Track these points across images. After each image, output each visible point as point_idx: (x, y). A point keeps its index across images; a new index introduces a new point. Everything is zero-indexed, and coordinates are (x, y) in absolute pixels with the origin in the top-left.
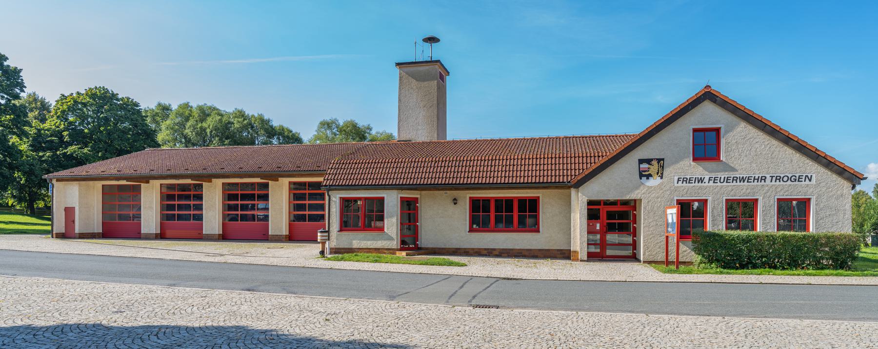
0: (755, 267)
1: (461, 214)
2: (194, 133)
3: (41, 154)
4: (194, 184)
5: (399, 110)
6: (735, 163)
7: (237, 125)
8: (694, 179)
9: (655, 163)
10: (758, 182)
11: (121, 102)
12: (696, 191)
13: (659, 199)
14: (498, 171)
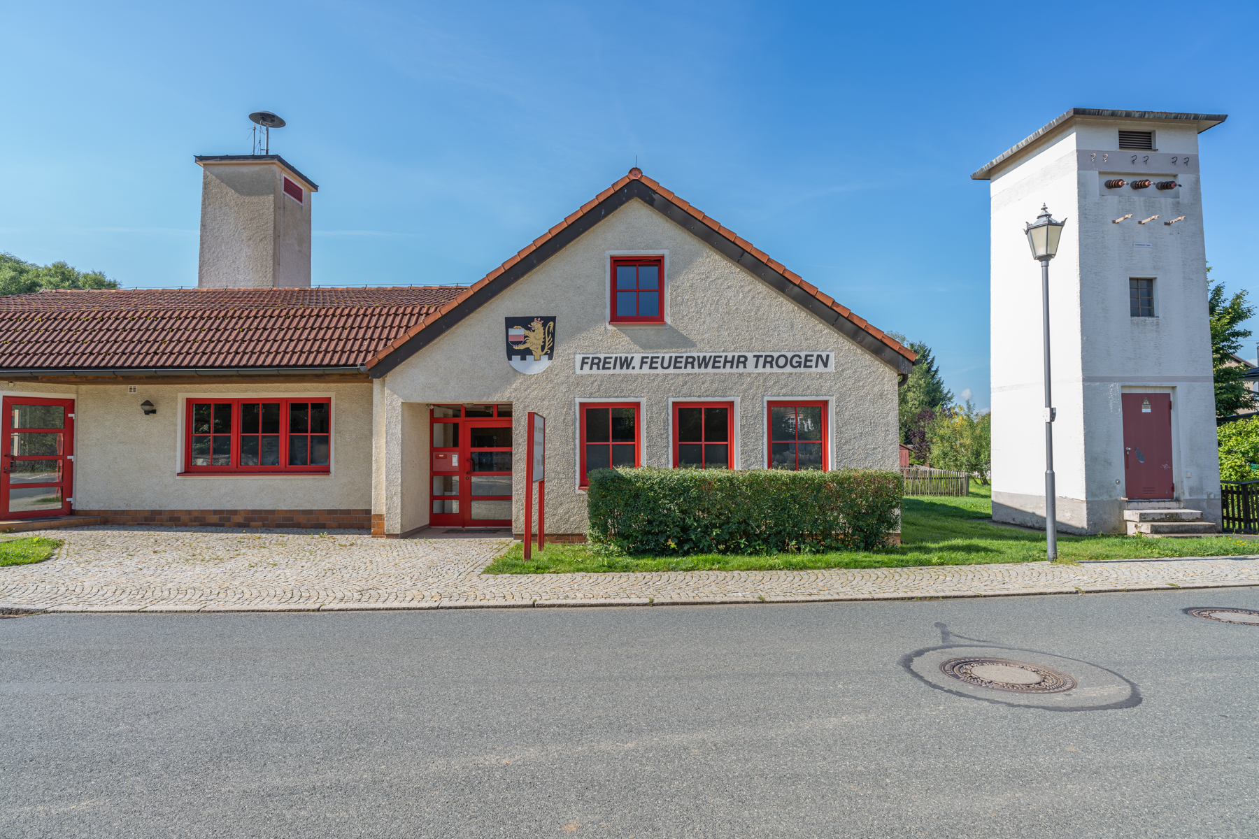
6: (690, 327)
8: (612, 361)
9: (537, 325)
10: (732, 367)
13: (546, 403)
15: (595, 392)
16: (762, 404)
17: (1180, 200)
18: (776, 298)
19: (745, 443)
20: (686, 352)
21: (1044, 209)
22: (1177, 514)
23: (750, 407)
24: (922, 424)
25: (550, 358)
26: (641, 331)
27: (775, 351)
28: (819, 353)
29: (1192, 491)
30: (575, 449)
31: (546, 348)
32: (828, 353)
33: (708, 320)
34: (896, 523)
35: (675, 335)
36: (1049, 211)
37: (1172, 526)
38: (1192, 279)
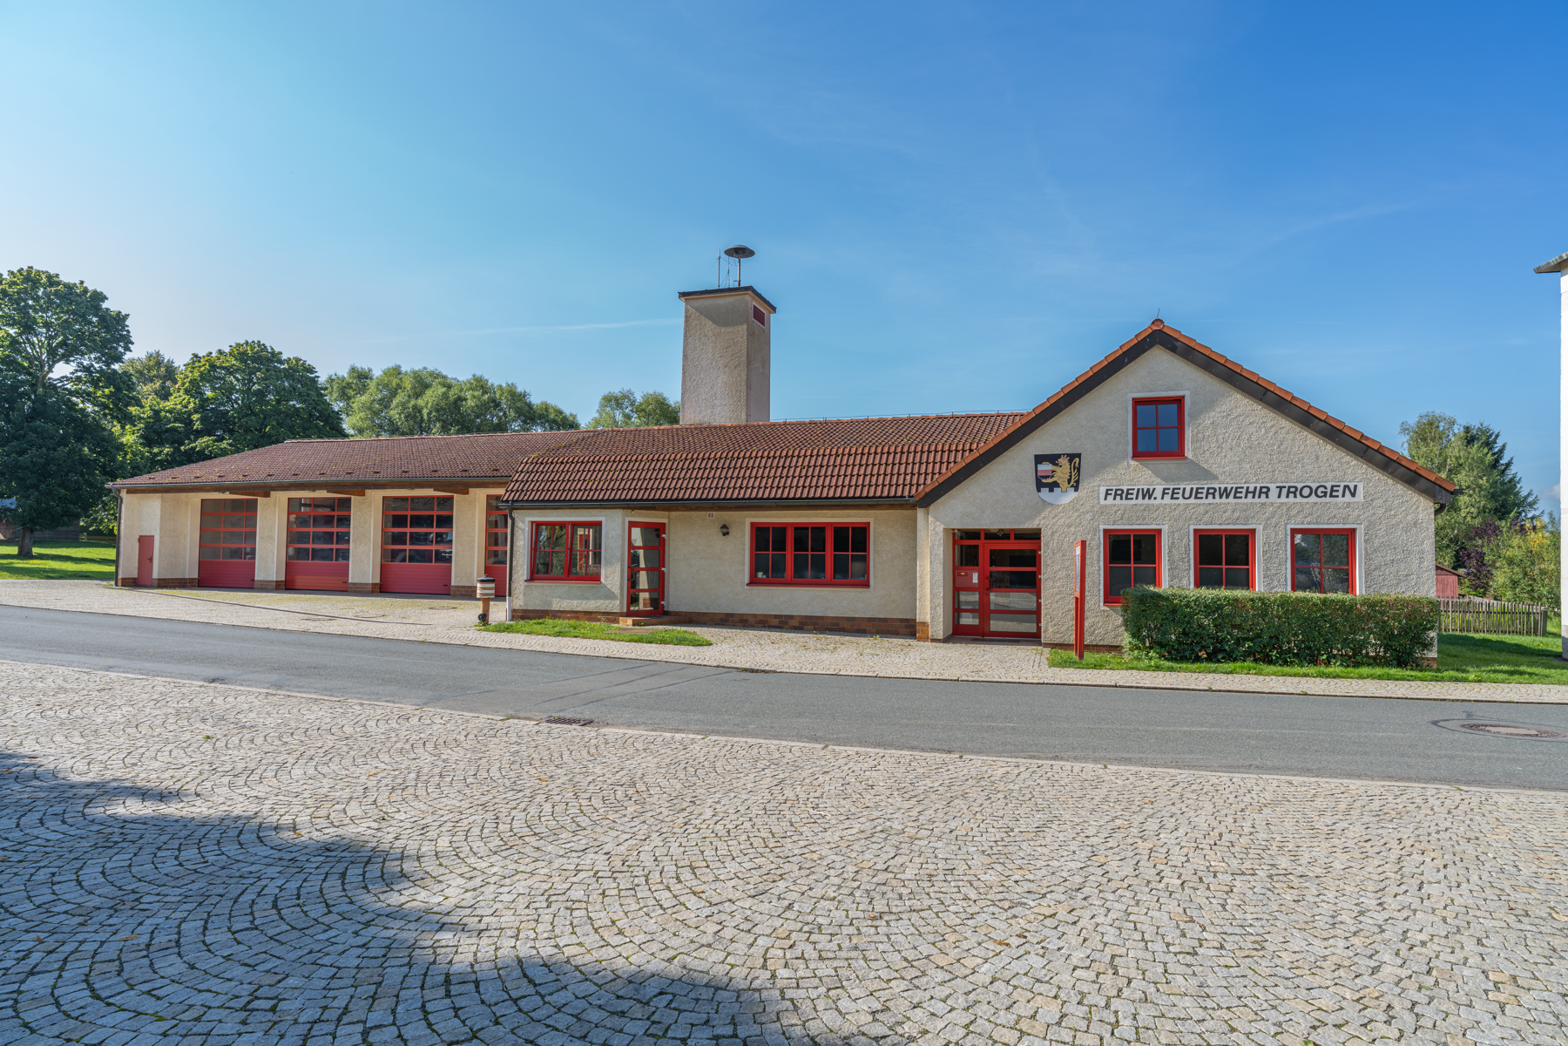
0: (1231, 657)
1: (739, 549)
2: (402, 416)
3: (156, 450)
4: (438, 497)
5: (684, 373)
6: (1211, 461)
7: (471, 403)
8: (1135, 492)
9: (1064, 461)
10: (1254, 497)
11: (286, 366)
12: (1139, 514)
13: (1072, 529)
14: (919, 474)
24: (1480, 542)
25: (1076, 490)
30: (1099, 570)
33: (1230, 454)
34: (1431, 644)
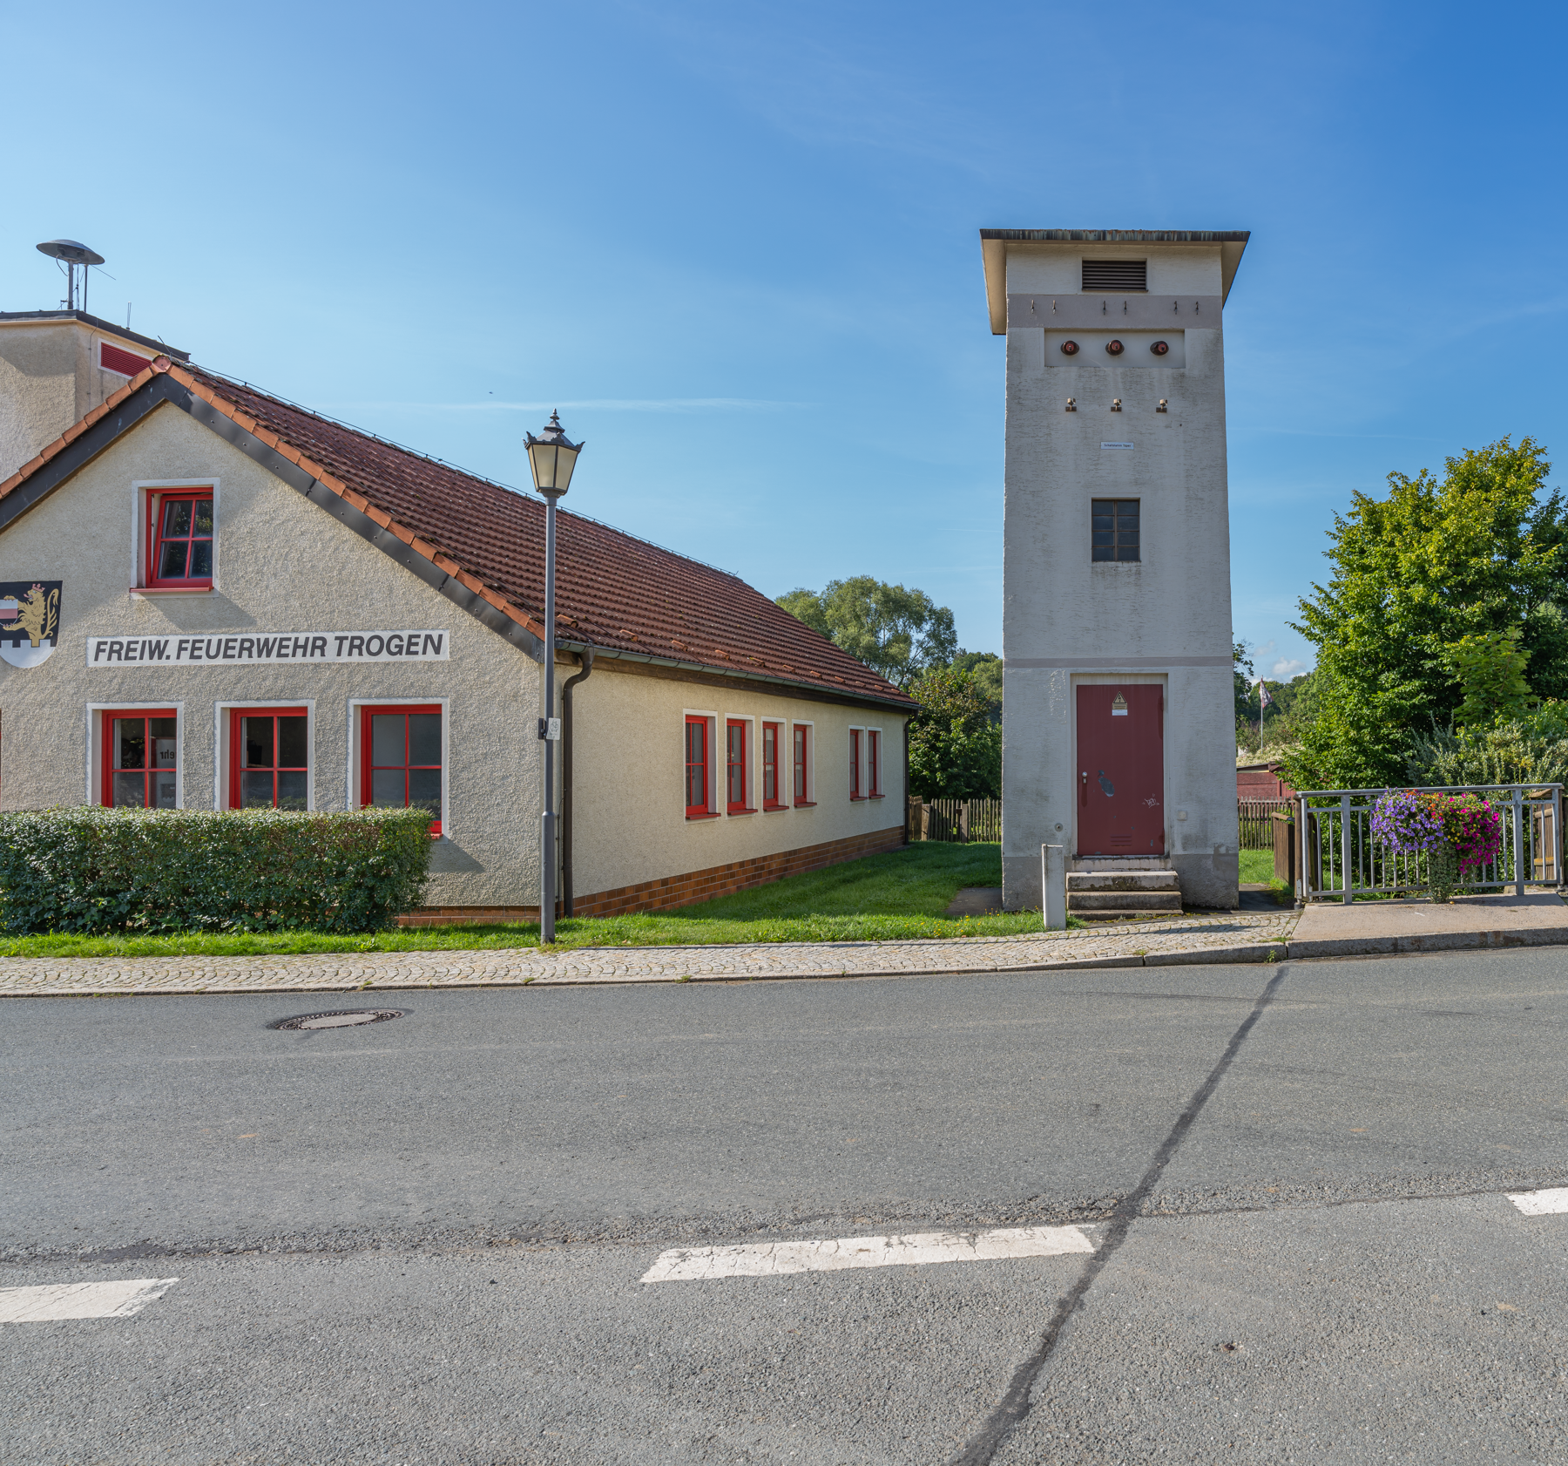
6: (247, 595)
8: (139, 647)
9: (36, 594)
10: (304, 655)
13: (46, 710)
15: (114, 694)
16: (347, 710)
17: (1186, 371)
18: (369, 548)
19: (321, 770)
20: (241, 633)
21: (555, 418)
22: (1132, 878)
23: (330, 715)
25: (53, 644)
26: (179, 602)
27: (365, 630)
28: (428, 632)
29: (1187, 842)
30: (85, 779)
31: (48, 628)
32: (441, 632)
35: (226, 607)
36: (562, 423)
37: (1104, 898)
38: (1202, 499)
